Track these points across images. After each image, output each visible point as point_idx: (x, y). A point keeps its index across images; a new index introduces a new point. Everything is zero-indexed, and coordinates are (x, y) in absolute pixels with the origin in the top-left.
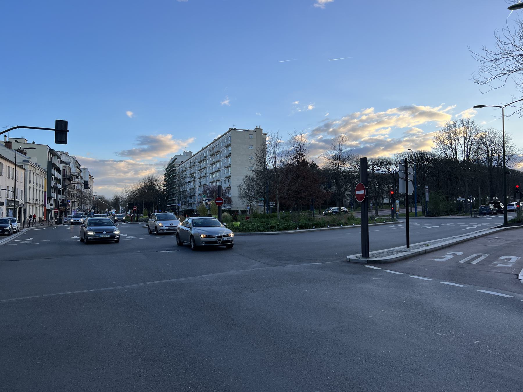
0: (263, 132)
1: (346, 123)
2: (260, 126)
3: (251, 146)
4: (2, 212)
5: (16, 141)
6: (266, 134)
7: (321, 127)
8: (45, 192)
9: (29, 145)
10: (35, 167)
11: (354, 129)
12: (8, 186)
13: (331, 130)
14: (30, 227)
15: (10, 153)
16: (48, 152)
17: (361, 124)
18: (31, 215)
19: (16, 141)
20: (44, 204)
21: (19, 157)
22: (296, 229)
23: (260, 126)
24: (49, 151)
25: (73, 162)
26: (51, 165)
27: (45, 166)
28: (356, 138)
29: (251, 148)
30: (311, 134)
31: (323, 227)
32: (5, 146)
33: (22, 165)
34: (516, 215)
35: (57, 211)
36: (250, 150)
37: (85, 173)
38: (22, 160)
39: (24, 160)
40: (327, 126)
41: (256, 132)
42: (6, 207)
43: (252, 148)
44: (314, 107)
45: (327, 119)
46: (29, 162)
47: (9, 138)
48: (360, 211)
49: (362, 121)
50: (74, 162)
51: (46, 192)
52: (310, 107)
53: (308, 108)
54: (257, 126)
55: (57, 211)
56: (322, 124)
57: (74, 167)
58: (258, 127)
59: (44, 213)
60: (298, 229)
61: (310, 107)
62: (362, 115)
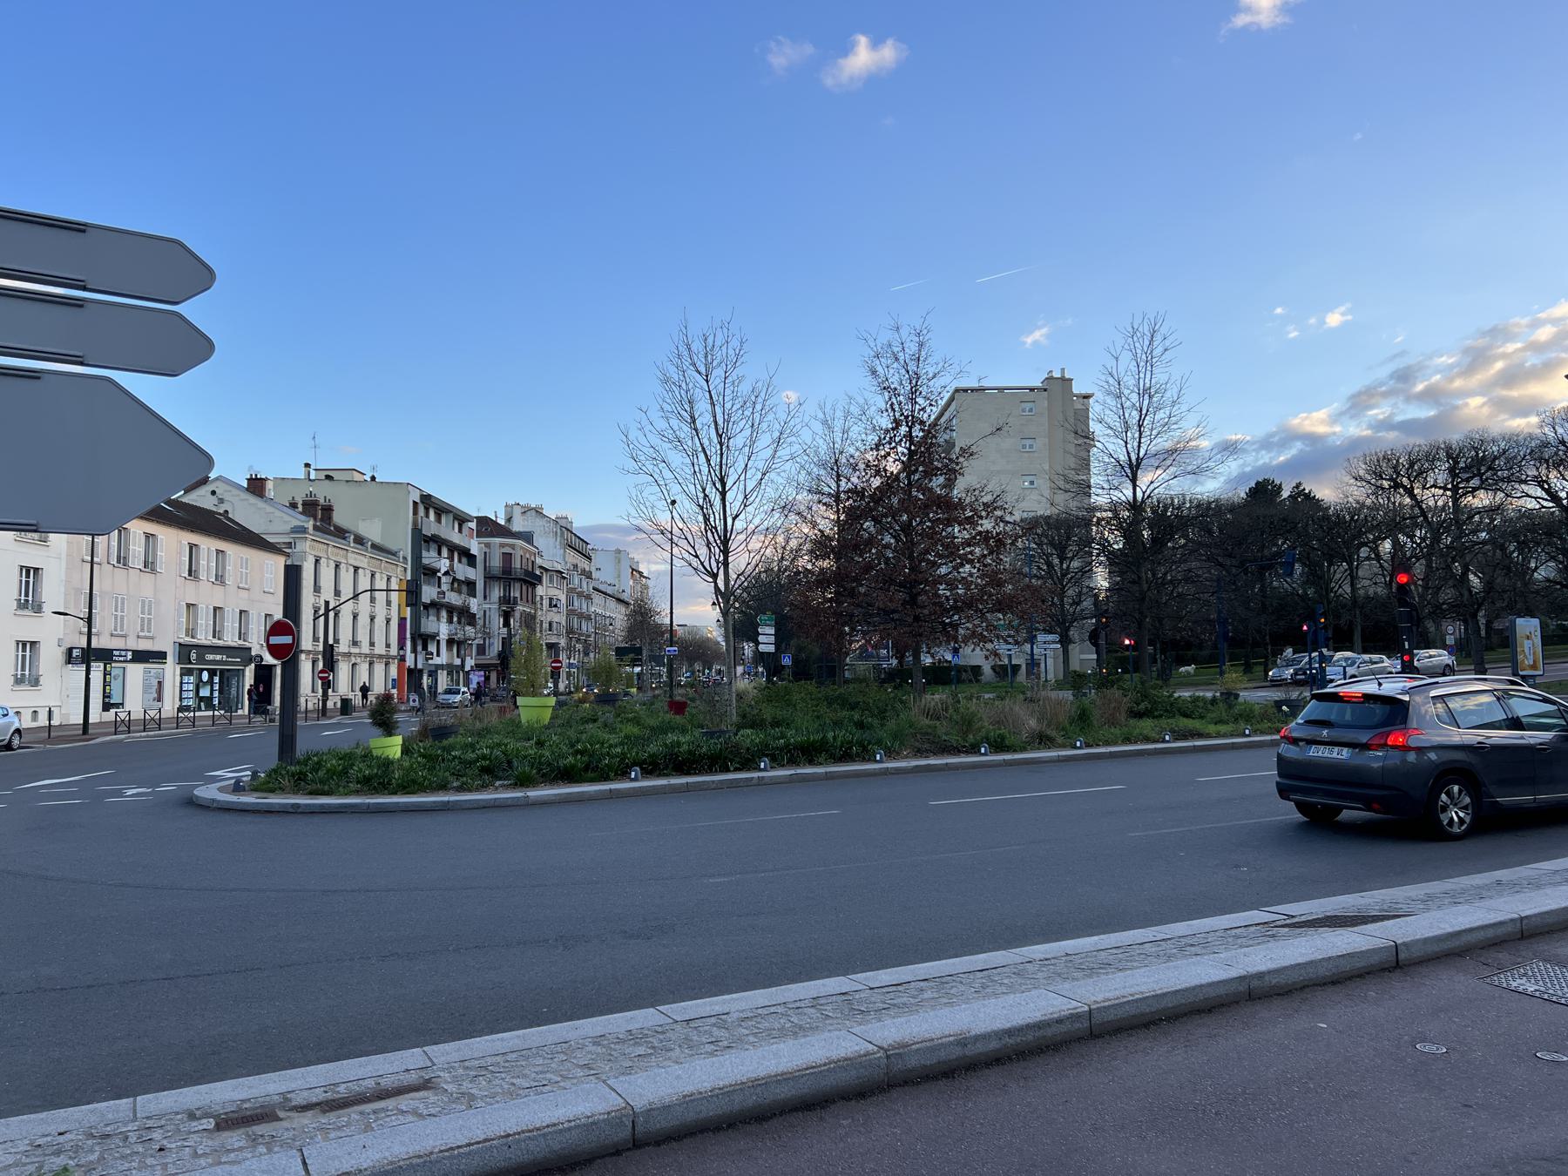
0: (1075, 390)
1: (1476, 358)
2: (1063, 370)
3: (1028, 442)
4: (160, 683)
5: (328, 477)
6: (1087, 397)
7: (1382, 384)
8: (402, 621)
9: (360, 486)
10: (346, 548)
11: (1511, 377)
12: (189, 606)
13: (1420, 387)
14: (116, 734)
15: (259, 509)
16: (415, 503)
17: (1532, 360)
18: (364, 683)
19: (328, 477)
20: (394, 651)
21: (282, 517)
22: (623, 773)
23: (1063, 370)
24: (418, 501)
25: (556, 532)
26: (422, 540)
27: (405, 546)
28: (1522, 409)
29: (1027, 450)
30: (1344, 408)
31: (846, 757)
32: (247, 489)
33: (288, 540)
34: (1328, 320)
35: (327, 675)
36: (1026, 455)
37: (619, 562)
38: (288, 528)
39: (295, 527)
40: (1404, 376)
41: (1045, 390)
42: (178, 668)
43: (1031, 446)
44: (1349, 317)
45: (1403, 353)
46: (308, 533)
47: (316, 470)
48: (1509, 661)
49: (1536, 347)
50: (559, 530)
51: (405, 619)
52: (1334, 319)
53: (1325, 323)
54: (1051, 372)
55: (327, 675)
56: (1384, 372)
57: (558, 547)
58: (1057, 374)
59: (330, 688)
60: (983, 750)
61: (1334, 319)
62: (1536, 324)
